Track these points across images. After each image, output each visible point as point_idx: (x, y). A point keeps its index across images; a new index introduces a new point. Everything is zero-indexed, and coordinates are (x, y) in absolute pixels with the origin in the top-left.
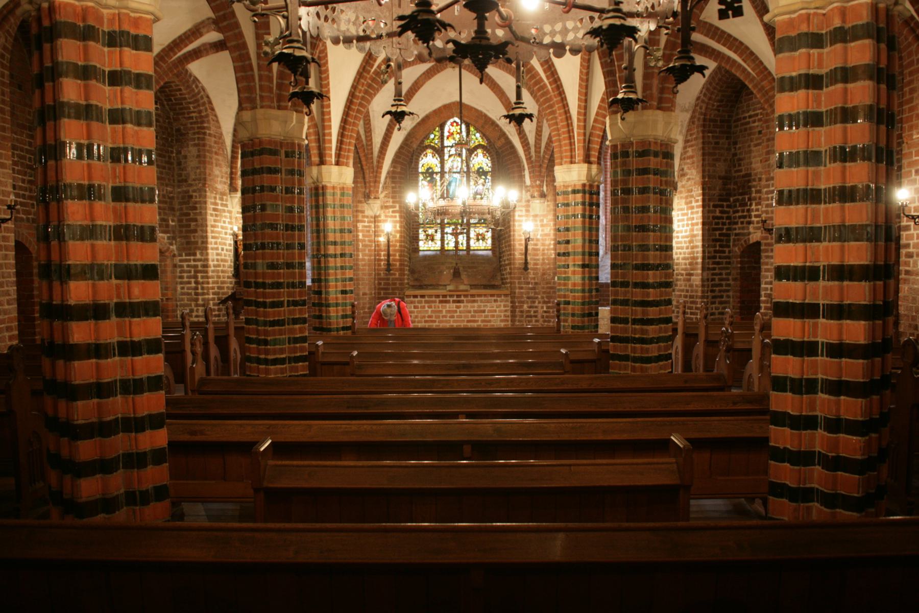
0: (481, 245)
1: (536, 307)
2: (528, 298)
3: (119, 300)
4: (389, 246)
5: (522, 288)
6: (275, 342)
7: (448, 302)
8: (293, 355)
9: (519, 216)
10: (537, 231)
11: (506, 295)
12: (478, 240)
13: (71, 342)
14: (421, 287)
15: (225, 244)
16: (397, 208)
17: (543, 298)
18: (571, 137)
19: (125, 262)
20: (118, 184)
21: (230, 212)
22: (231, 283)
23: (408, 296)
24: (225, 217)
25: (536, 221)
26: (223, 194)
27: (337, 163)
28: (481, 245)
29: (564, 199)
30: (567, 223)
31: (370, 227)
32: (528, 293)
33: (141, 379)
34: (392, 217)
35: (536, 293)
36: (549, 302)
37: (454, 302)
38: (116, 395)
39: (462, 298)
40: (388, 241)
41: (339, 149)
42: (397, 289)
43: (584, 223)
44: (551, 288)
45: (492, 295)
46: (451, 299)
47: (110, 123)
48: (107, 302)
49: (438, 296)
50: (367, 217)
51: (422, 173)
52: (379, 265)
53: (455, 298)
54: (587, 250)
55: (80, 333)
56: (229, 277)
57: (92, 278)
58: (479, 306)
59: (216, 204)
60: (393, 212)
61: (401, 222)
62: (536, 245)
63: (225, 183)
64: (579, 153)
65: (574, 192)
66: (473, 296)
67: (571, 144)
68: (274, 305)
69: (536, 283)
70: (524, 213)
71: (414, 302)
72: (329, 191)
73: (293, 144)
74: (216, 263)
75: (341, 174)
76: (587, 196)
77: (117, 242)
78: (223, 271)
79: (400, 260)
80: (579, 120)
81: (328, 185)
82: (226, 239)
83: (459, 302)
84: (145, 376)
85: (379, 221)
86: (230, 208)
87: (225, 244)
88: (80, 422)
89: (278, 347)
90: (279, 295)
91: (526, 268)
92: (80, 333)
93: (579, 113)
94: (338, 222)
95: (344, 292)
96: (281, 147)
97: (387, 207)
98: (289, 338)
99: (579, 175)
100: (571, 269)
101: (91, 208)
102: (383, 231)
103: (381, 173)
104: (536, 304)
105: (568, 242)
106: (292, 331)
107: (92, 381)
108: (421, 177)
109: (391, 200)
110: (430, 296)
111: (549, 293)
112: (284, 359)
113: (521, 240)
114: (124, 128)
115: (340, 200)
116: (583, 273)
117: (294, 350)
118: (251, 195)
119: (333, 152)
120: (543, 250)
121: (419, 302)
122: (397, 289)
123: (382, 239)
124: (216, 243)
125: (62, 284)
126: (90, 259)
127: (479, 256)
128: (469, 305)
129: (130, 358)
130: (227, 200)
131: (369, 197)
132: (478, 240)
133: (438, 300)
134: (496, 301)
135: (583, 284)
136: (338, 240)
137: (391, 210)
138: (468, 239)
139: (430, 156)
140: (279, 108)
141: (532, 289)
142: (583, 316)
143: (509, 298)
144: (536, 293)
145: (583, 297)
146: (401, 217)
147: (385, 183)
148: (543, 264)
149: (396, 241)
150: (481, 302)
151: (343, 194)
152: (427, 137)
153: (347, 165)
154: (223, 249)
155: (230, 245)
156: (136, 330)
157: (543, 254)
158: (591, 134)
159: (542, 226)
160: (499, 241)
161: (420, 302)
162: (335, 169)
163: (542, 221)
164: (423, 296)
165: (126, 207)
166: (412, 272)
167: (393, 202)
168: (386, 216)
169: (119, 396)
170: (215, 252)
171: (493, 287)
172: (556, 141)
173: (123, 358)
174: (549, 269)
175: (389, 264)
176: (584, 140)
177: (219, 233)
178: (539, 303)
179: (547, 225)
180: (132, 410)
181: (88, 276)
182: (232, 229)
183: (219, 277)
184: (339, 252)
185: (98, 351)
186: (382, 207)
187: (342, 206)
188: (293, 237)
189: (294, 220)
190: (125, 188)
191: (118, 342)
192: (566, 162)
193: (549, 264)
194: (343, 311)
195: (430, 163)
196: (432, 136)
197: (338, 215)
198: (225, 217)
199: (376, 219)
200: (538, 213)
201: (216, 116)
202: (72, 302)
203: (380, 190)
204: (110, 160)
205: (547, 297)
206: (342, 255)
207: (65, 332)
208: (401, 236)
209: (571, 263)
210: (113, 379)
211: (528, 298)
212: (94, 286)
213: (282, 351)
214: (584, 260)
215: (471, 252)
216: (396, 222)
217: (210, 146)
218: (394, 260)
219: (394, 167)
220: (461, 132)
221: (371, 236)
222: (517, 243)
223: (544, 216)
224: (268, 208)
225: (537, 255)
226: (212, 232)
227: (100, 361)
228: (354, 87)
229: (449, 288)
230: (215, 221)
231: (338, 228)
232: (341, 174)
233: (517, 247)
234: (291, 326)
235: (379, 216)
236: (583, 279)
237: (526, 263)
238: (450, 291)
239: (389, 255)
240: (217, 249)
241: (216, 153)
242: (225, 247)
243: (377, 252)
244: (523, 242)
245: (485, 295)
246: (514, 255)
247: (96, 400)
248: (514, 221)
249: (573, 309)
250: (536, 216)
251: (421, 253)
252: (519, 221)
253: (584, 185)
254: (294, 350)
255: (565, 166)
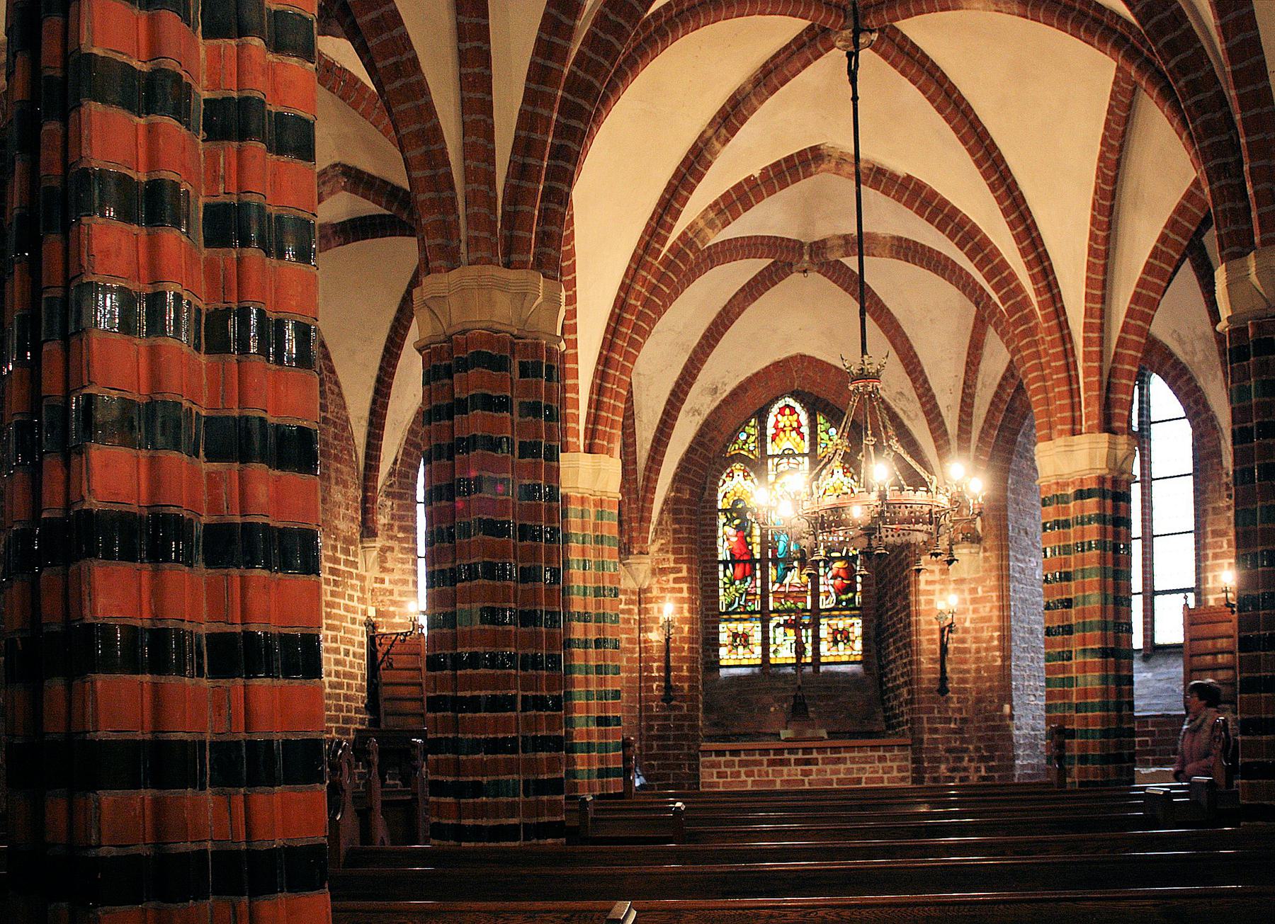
0: (843, 652)
1: (965, 769)
2: (948, 750)
3: (215, 519)
4: (668, 651)
5: (935, 731)
6: (497, 789)
7: (785, 763)
8: (534, 820)
9: (928, 582)
10: (965, 611)
11: (903, 747)
12: (836, 642)
13: (89, 619)
14: (725, 738)
15: (351, 643)
16: (684, 574)
17: (977, 749)
18: (1071, 380)
19: (236, 413)
20: (222, 199)
21: (362, 578)
22: (362, 721)
23: (707, 753)
24: (353, 587)
25: (963, 591)
26: (349, 541)
27: (590, 449)
28: (843, 652)
29: (1058, 512)
30: (1066, 563)
31: (630, 611)
32: (948, 740)
33: (269, 743)
34: (673, 590)
35: (963, 740)
36: (992, 758)
37: (798, 762)
38: (203, 788)
39: (815, 755)
40: (668, 640)
41: (593, 419)
42: (686, 737)
43: (1103, 559)
44: (994, 728)
45: (874, 748)
46: (793, 757)
47: (206, 36)
48: (186, 514)
49: (765, 752)
50: (625, 592)
51: (725, 511)
52: (650, 689)
53: (800, 756)
54: (1110, 619)
55: (115, 594)
56: (357, 710)
57: (151, 442)
58: (849, 771)
59: (337, 561)
60: (676, 580)
61: (691, 601)
62: (963, 641)
63: (353, 520)
64: (1089, 410)
65: (1081, 495)
66: (835, 749)
67: (1073, 393)
68: (497, 704)
69: (964, 720)
70: (937, 576)
71: (718, 765)
72: (574, 508)
73: (537, 346)
74: (334, 679)
75: (597, 472)
76: (1109, 502)
77: (215, 357)
78: (347, 698)
79: (690, 679)
80: (1087, 341)
81: (572, 493)
82: (353, 632)
83: (807, 762)
84: (278, 737)
85: (649, 601)
86: (361, 571)
87: (351, 643)
88: (103, 851)
89: (504, 799)
90: (507, 682)
91: (943, 690)
92: (115, 594)
93: (1087, 327)
94: (591, 572)
95: (602, 721)
96: (513, 353)
97: (663, 571)
98: (526, 782)
99: (1092, 459)
100: (1077, 660)
101: (153, 246)
102: (656, 620)
103: (652, 501)
104: (965, 763)
105: (1068, 603)
106: (532, 766)
107: (139, 737)
108: (722, 519)
109: (672, 557)
110: (750, 752)
111: (991, 739)
112: (516, 827)
113: (931, 632)
114: (241, 48)
115: (596, 527)
116: (1105, 667)
117: (537, 809)
118: (444, 461)
119: (582, 427)
120: (978, 651)
121: (727, 764)
122: (686, 737)
123: (655, 636)
124: (334, 639)
125: (67, 465)
126: (144, 390)
127: (837, 674)
128: (828, 767)
129: (240, 681)
130: (355, 555)
131: (630, 553)
132: (836, 642)
133: (765, 759)
134: (882, 759)
135: (1105, 692)
136: (592, 610)
137: (672, 576)
138: (817, 640)
139: (738, 474)
140: (508, 265)
141: (954, 732)
142: (1105, 759)
143: (909, 753)
144: (963, 740)
145: (1105, 720)
146: (691, 590)
147: (660, 523)
148: (978, 679)
149: (682, 640)
150: (853, 761)
151: (600, 515)
152: (733, 438)
153: (609, 452)
154: (347, 654)
155: (361, 645)
156: (258, 602)
157: (978, 660)
158: (1113, 373)
159: (974, 601)
160: (879, 643)
161: (729, 764)
162: (585, 460)
163: (974, 590)
164: (735, 753)
165: (240, 261)
166: (708, 709)
167: (676, 561)
168: (663, 590)
169: (209, 790)
170: (333, 656)
171: (870, 735)
172: (1036, 392)
173: (222, 682)
174: (991, 689)
175: (668, 688)
176: (1101, 382)
177: (342, 618)
178: (971, 760)
179: (983, 600)
180: (243, 837)
181: (139, 436)
182: (365, 613)
183: (339, 708)
184: (592, 636)
185: (156, 650)
186: (653, 573)
187: (599, 540)
188: (535, 552)
189: (537, 517)
190: (243, 207)
191: (210, 637)
192: (1061, 433)
193: (991, 679)
194: (601, 761)
195: (739, 489)
196: (743, 437)
197: (591, 556)
198: (353, 587)
199: (642, 596)
200: (965, 576)
201: (337, 384)
202: (94, 504)
203: (651, 536)
204: (202, 135)
205: (988, 748)
206: (599, 643)
207: (72, 596)
208: (691, 631)
209: (1076, 648)
210: (197, 738)
211: (948, 750)
212: (153, 462)
213: (512, 810)
214: (1104, 639)
215: (822, 669)
216: (681, 600)
217: (326, 444)
218: (681, 679)
219: (678, 490)
220: (800, 425)
221: (630, 631)
222: (923, 638)
223: (979, 580)
224: (485, 487)
225: (965, 661)
226: (329, 616)
227: (163, 679)
228: (625, 288)
229: (784, 734)
230: (333, 594)
231: (591, 585)
232: (597, 472)
233: (925, 645)
234: (531, 755)
235: (648, 590)
236: (1104, 680)
237: (943, 678)
238: (787, 740)
239: (668, 669)
240: (337, 651)
241: (337, 458)
242: (352, 649)
243: (644, 664)
244: (937, 636)
245: (860, 748)
246: (919, 663)
247: (148, 794)
248: (917, 592)
249: (1083, 747)
250: (961, 581)
251: (723, 672)
252: (931, 593)
253: (1101, 480)
254: (537, 809)
255: (1060, 441)
